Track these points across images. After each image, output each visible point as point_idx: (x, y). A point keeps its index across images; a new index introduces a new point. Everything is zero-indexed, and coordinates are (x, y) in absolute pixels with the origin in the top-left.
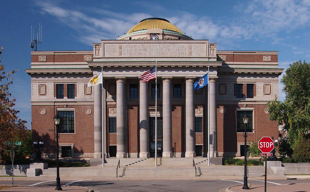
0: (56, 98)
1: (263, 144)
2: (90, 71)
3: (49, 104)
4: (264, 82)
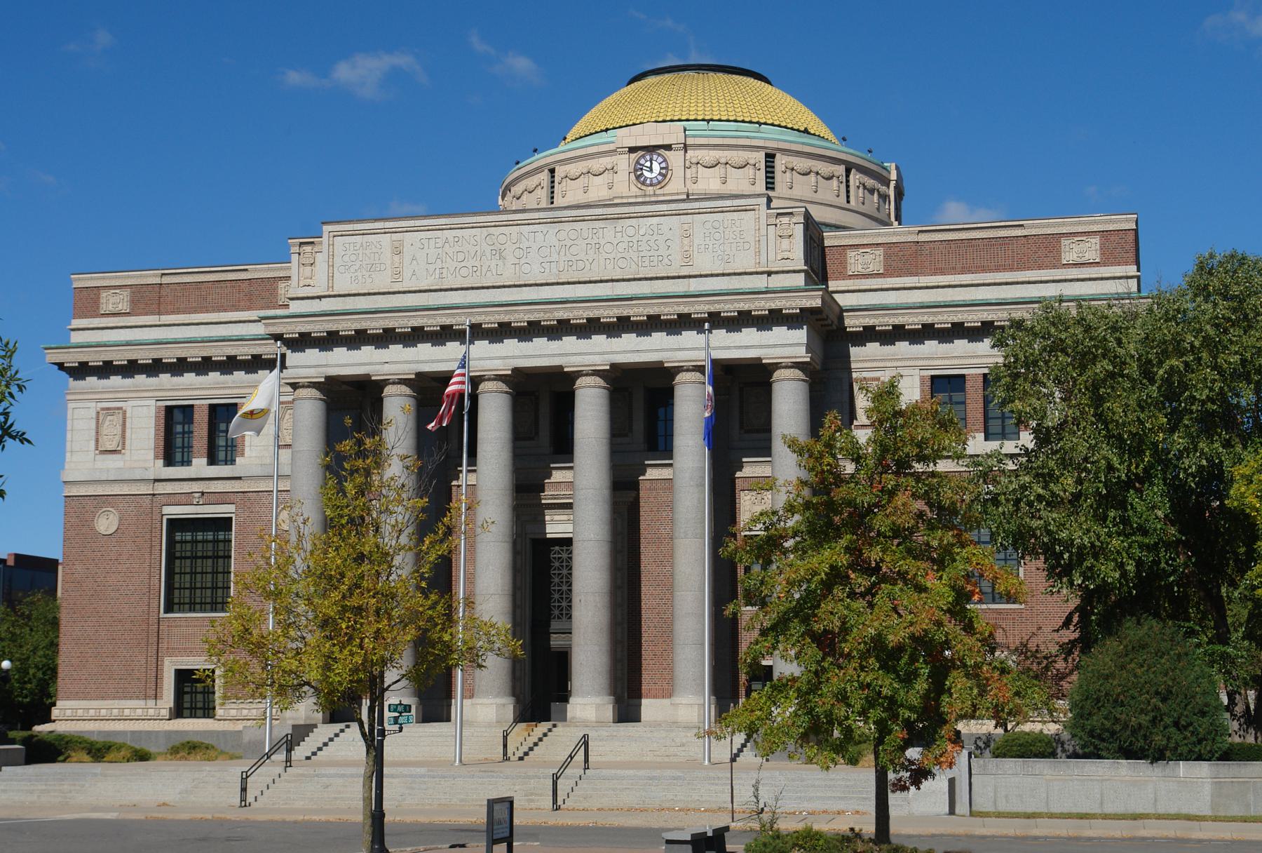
0: (161, 462)
2: (272, 349)
3: (135, 489)
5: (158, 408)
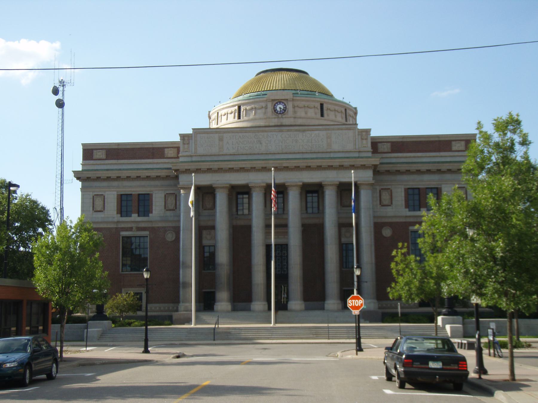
0: (119, 215)
1: (352, 302)
3: (109, 226)
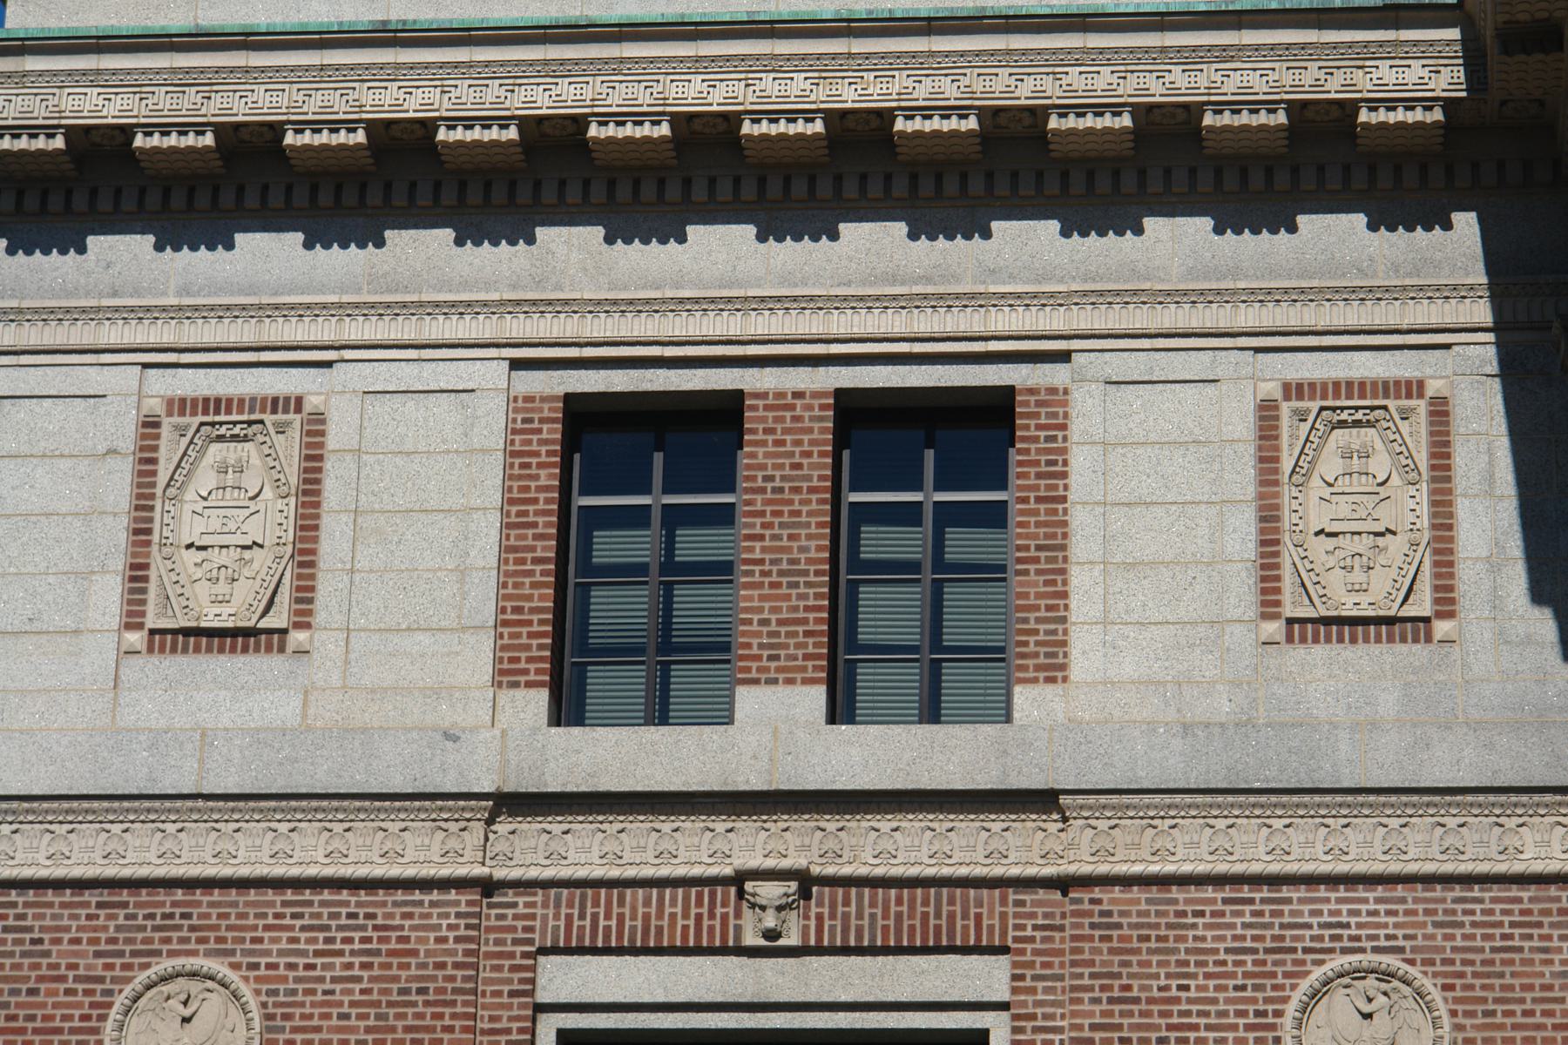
4: (1269, 342)
5: (522, 408)
